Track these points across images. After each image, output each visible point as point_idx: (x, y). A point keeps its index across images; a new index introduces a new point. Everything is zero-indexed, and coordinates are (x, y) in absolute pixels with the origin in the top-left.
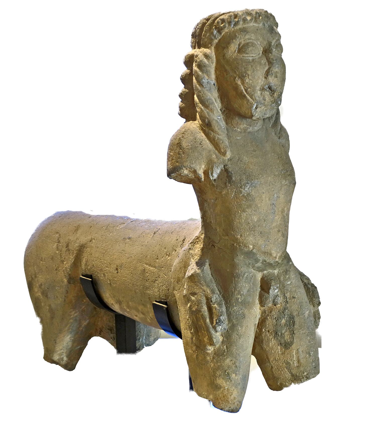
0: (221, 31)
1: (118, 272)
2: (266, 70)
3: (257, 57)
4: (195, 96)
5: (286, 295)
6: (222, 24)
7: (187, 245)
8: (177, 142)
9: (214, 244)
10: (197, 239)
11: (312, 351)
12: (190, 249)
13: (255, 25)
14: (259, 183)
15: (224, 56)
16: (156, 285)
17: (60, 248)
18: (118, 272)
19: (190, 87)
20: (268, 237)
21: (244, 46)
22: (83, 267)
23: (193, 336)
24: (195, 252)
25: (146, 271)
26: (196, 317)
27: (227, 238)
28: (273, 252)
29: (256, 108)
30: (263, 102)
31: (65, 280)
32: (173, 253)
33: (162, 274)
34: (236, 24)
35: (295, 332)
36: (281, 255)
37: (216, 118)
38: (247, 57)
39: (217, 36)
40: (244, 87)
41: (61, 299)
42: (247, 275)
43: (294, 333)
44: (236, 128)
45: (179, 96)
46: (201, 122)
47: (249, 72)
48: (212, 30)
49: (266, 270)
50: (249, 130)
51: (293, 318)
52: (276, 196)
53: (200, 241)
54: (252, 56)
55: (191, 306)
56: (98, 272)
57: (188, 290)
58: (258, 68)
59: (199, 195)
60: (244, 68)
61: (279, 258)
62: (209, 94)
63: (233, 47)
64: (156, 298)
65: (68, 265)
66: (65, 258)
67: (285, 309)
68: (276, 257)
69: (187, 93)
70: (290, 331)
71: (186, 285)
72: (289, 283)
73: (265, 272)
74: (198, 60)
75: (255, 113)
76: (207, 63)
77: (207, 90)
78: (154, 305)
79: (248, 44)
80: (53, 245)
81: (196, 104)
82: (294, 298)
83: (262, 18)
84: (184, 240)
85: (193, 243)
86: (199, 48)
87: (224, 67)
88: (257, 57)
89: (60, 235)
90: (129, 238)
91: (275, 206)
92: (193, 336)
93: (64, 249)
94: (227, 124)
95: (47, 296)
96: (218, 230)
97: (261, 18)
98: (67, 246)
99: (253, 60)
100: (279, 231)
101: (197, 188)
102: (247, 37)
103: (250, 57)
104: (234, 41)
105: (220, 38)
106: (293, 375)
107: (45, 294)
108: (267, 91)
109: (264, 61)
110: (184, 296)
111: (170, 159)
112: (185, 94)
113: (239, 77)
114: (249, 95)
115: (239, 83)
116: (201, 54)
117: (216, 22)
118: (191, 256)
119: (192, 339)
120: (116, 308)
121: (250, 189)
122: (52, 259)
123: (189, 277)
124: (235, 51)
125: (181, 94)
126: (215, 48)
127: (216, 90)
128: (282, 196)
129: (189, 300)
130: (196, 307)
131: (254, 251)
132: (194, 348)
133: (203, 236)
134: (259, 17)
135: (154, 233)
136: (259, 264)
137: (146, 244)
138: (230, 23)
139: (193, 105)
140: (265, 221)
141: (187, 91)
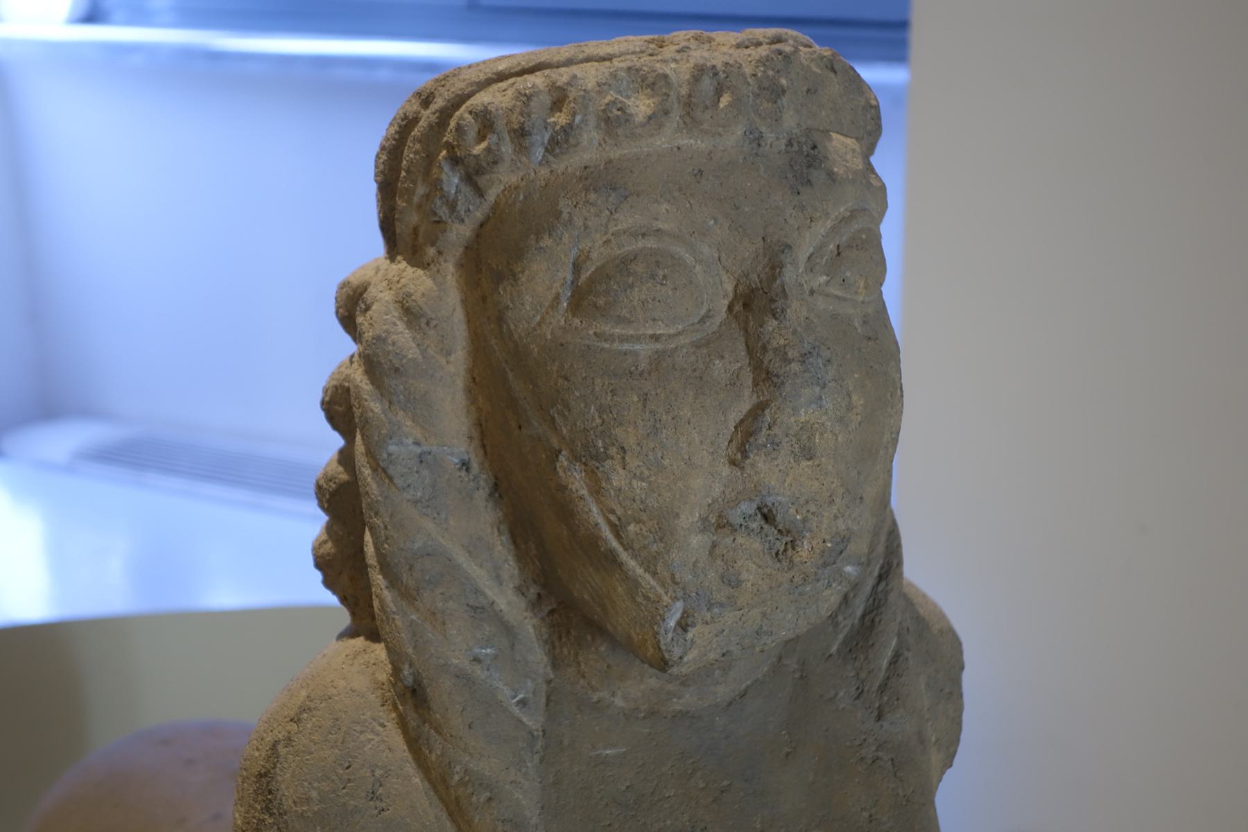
0: (482, 181)
2: (735, 416)
3: (684, 340)
6: (481, 137)
13: (684, 141)
15: (500, 320)
21: (602, 275)
29: (683, 626)
30: (720, 597)
34: (560, 142)
37: (459, 660)
38: (624, 339)
39: (461, 207)
40: (607, 511)
44: (603, 694)
47: (629, 437)
48: (435, 170)
50: (677, 705)
54: (656, 338)
58: (686, 413)
60: (601, 410)
62: (428, 525)
63: (542, 284)
75: (677, 651)
76: (413, 352)
77: (416, 502)
79: (625, 263)
83: (736, 103)
88: (684, 340)
94: (555, 664)
97: (725, 100)
99: (659, 357)
102: (627, 219)
103: (638, 339)
104: (547, 242)
105: (479, 215)
108: (749, 531)
109: (731, 362)
113: (576, 458)
114: (635, 557)
115: (577, 481)
116: (388, 296)
124: (557, 297)
126: (460, 266)
127: (481, 495)
134: (719, 93)
138: (521, 134)
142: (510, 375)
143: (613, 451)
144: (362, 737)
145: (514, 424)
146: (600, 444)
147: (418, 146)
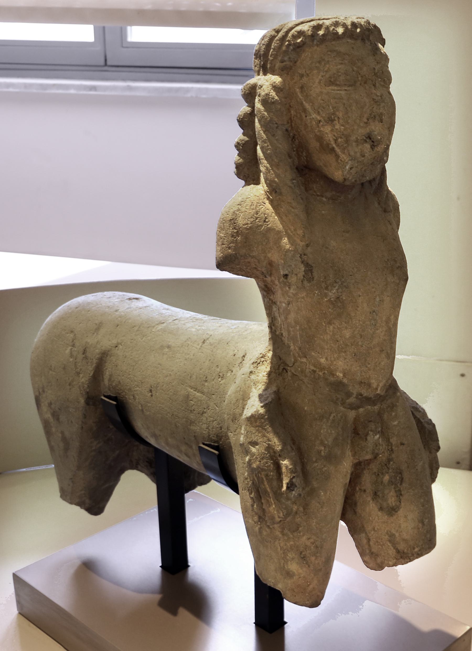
1: (152, 396)
4: (258, 147)
5: (391, 440)
7: (248, 365)
8: (230, 217)
9: (286, 367)
10: (262, 357)
11: (426, 519)
12: (251, 372)
14: (353, 281)
16: (205, 419)
17: (75, 353)
18: (152, 396)
19: (251, 133)
20: (366, 360)
22: (106, 382)
23: (254, 502)
24: (259, 378)
25: (191, 397)
26: (258, 478)
27: (304, 360)
28: (373, 381)
31: (82, 401)
32: (229, 374)
33: (212, 404)
35: (402, 493)
36: (385, 385)
41: (77, 426)
42: (334, 417)
43: (401, 495)
45: (236, 146)
46: (266, 188)
49: (362, 407)
51: (401, 473)
52: (378, 299)
53: (266, 361)
54: (346, 90)
55: (250, 460)
56: (126, 393)
57: (246, 436)
59: (265, 293)
61: (381, 390)
64: (204, 438)
65: (84, 379)
66: (81, 370)
67: (389, 460)
68: (377, 389)
69: (247, 142)
70: (396, 491)
71: (243, 428)
72: (396, 423)
73: (361, 410)
74: (263, 93)
78: (200, 448)
80: (66, 349)
81: (260, 159)
82: (402, 444)
84: (244, 356)
85: (257, 363)
86: (265, 74)
87: (302, 104)
89: (75, 335)
90: (169, 347)
91: (377, 315)
92: (254, 502)
93: (81, 356)
95: (58, 419)
96: (292, 347)
98: (84, 352)
100: (382, 351)
101: (262, 284)
106: (398, 552)
107: (55, 415)
110: (241, 445)
111: (220, 243)
112: (243, 144)
117: (290, 35)
118: (252, 384)
119: (252, 506)
120: (152, 441)
121: (340, 290)
122: (64, 368)
123: (247, 418)
125: (238, 143)
128: (387, 299)
129: (247, 452)
130: (258, 463)
131: (345, 381)
132: (256, 518)
133: (270, 354)
135: (204, 342)
136: (352, 400)
137: (192, 357)
139: (255, 161)
140: (361, 337)
141: (247, 139)
142: (304, 102)
143: (336, 118)
144: (261, 207)
145: (304, 116)
146: (333, 117)
147: (278, 42)
